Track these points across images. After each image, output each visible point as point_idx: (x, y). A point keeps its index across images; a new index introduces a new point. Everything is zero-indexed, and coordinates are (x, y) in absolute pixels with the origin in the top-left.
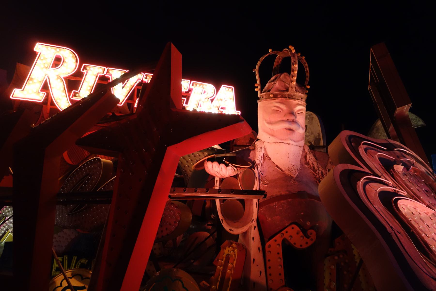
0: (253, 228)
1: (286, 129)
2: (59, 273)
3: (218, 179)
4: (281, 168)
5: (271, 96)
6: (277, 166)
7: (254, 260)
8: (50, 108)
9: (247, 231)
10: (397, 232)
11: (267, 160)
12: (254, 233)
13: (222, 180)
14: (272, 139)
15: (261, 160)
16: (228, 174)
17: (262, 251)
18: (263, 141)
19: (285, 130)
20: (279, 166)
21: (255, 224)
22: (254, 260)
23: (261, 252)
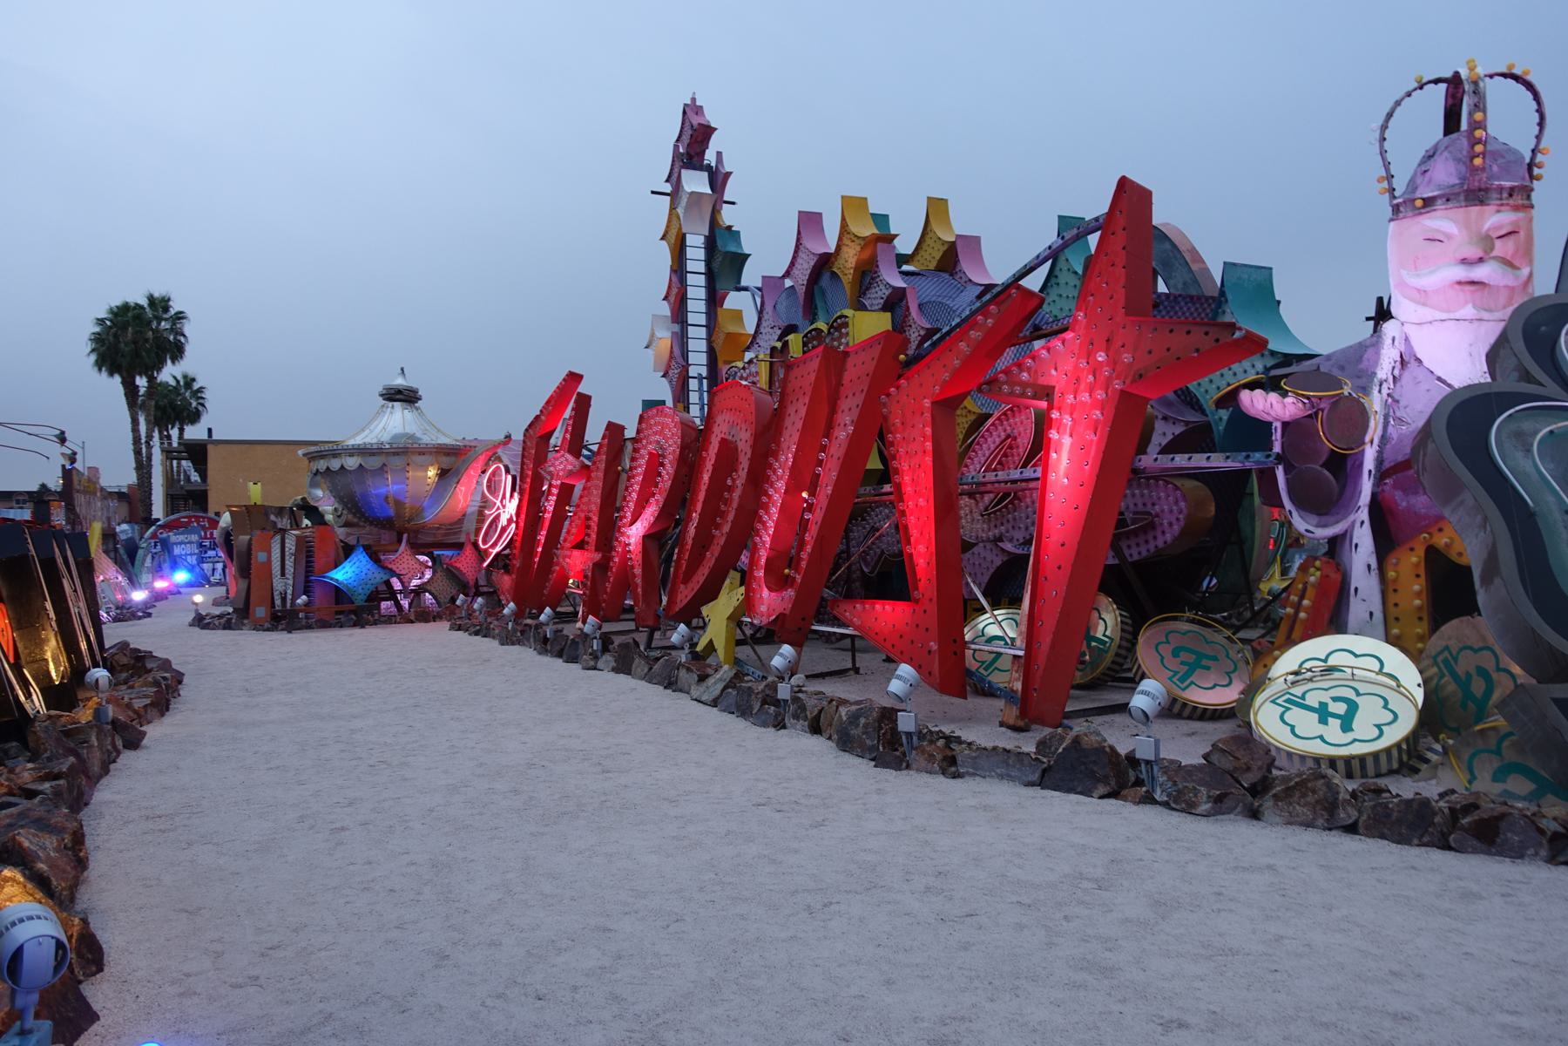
0: (1358, 524)
1: (1459, 283)
2: (441, 514)
3: (1278, 425)
4: (1449, 382)
5: (1419, 203)
6: (1439, 379)
7: (1356, 589)
8: (98, 1018)
9: (1346, 531)
10: (1492, 531)
11: (1413, 364)
12: (1363, 538)
13: (1285, 425)
14: (1427, 313)
15: (1394, 368)
16: (1287, 413)
17: (1377, 571)
18: (1403, 319)
19: (1457, 287)
20: (1443, 377)
21: (1364, 514)
22: (1356, 589)
23: (1375, 573)
